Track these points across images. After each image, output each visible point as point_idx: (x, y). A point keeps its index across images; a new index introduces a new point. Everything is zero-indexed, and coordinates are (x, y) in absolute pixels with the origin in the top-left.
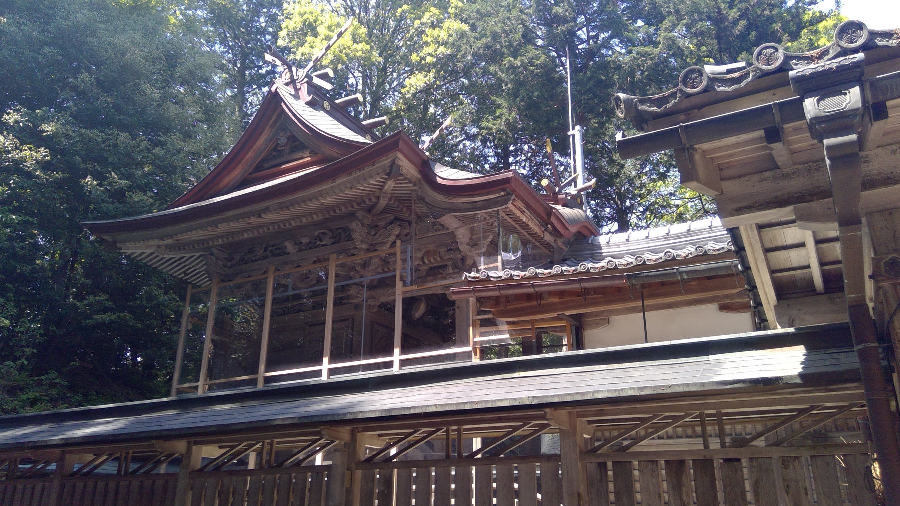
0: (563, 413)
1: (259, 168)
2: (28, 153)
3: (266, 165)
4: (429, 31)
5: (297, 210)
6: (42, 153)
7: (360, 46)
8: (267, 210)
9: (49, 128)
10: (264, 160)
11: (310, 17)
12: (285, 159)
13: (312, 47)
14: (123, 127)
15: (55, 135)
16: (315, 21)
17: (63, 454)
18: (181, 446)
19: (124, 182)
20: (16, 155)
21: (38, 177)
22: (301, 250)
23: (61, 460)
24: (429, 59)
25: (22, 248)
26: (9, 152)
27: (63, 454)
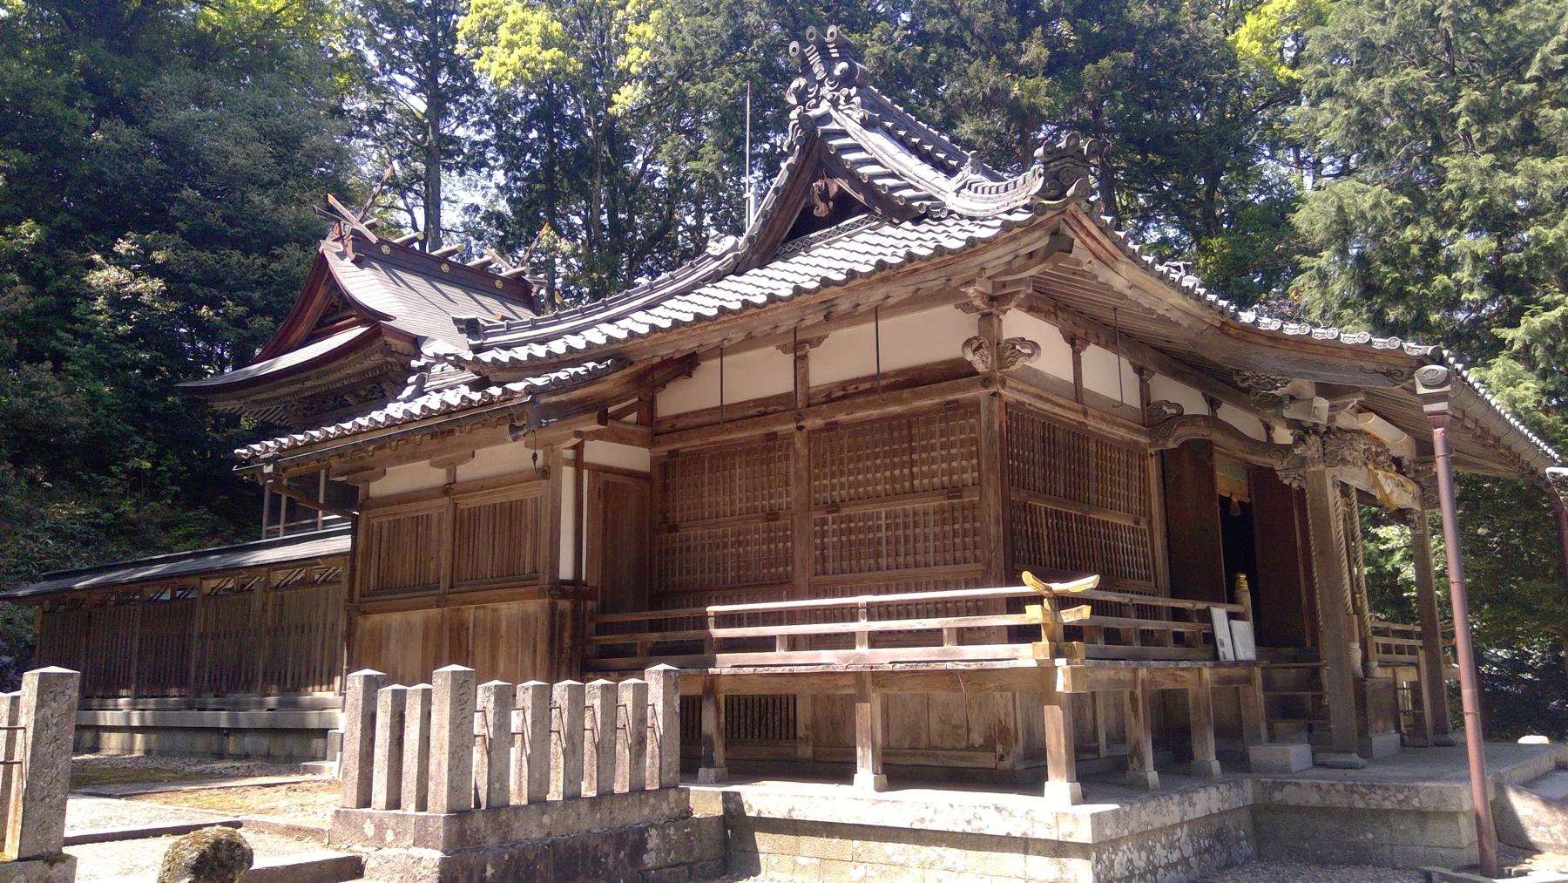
0: (265, 569)
1: (320, 324)
2: (143, 285)
3: (326, 321)
4: (632, 27)
5: (331, 378)
6: (158, 284)
7: (548, 54)
8: (307, 379)
9: (159, 257)
10: (325, 316)
11: (490, 12)
12: (335, 318)
13: (491, 61)
14: (235, 243)
15: (165, 263)
16: (497, 17)
17: (142, 587)
18: (196, 580)
19: (241, 309)
20: (132, 288)
21: (157, 309)
22: (360, 402)
23: (141, 592)
24: (633, 69)
25: (153, 386)
26: (125, 285)
27: (142, 587)
